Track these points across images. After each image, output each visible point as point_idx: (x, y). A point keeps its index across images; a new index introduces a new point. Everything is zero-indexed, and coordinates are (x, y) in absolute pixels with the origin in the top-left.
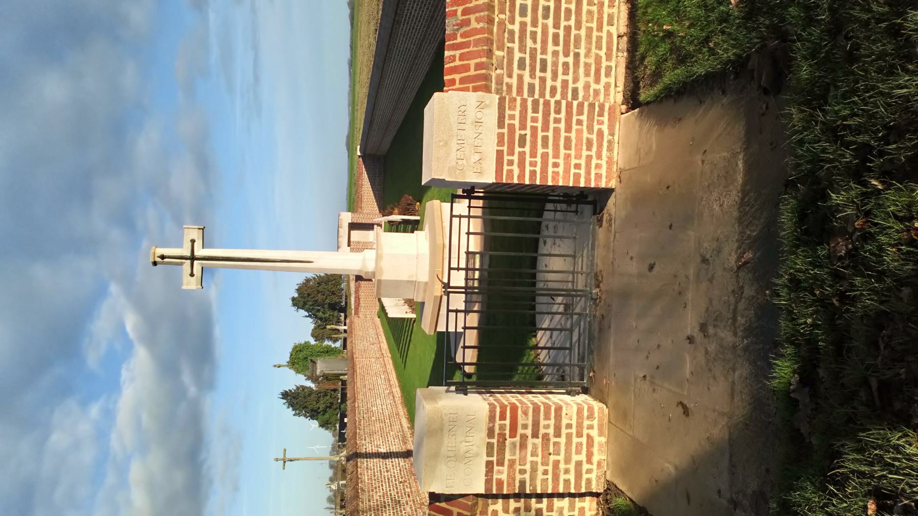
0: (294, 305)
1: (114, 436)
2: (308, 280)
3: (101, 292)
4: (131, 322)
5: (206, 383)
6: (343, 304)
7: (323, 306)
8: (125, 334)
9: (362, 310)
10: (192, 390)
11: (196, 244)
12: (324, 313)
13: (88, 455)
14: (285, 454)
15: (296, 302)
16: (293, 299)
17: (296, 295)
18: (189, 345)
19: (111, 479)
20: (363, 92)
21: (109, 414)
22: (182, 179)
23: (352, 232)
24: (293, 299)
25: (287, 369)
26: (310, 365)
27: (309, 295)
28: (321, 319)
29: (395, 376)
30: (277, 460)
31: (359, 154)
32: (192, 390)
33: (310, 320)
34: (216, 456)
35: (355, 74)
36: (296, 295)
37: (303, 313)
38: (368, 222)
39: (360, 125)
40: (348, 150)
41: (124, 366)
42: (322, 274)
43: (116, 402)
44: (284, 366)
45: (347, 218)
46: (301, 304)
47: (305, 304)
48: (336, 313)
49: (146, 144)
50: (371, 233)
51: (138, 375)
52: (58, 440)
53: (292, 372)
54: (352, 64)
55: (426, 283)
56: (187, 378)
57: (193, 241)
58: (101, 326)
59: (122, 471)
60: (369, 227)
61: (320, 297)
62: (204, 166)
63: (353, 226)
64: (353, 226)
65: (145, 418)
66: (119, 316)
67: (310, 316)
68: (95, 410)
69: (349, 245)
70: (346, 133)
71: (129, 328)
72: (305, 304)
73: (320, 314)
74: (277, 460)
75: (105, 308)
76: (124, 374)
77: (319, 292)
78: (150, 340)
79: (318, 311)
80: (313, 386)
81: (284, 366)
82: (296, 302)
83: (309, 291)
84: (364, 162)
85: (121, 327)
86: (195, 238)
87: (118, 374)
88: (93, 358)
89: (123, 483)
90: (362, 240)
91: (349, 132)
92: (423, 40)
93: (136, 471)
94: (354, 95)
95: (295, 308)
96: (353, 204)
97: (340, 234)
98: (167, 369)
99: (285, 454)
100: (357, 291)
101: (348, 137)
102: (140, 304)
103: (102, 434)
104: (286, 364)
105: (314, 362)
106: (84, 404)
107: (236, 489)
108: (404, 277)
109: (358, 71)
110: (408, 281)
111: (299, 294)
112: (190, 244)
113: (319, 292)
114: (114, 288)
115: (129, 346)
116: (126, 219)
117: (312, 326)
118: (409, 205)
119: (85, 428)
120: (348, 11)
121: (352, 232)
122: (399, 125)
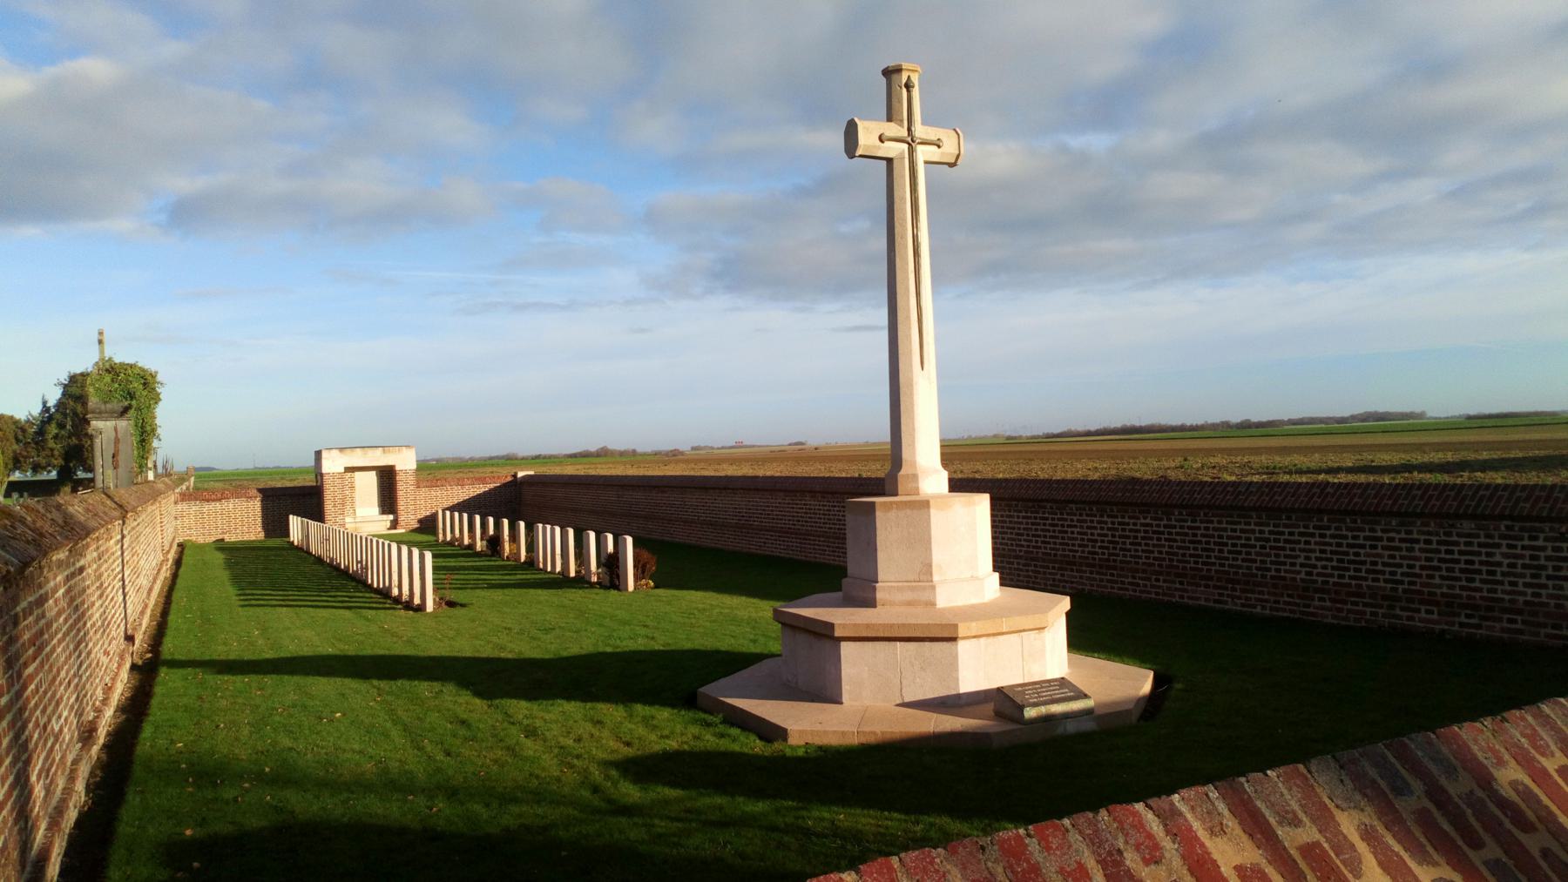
4: (96, 69)
8: (74, 53)
12: (56, 437)
22: (364, 180)
23: (373, 473)
26: (117, 405)
28: (41, 432)
31: (520, 474)
33: (36, 410)
37: (54, 396)
39: (569, 470)
44: (102, 351)
45: (405, 462)
48: (60, 462)
49: (450, 124)
50: (376, 510)
54: (585, 455)
55: (933, 604)
62: (388, 218)
64: (387, 477)
67: (46, 409)
73: (53, 429)
79: (61, 426)
81: (102, 351)
90: (358, 495)
94: (478, 466)
95: (64, 379)
96: (431, 472)
97: (370, 452)
108: (938, 556)
110: (930, 566)
114: (173, 50)
120: (593, 448)
121: (373, 473)
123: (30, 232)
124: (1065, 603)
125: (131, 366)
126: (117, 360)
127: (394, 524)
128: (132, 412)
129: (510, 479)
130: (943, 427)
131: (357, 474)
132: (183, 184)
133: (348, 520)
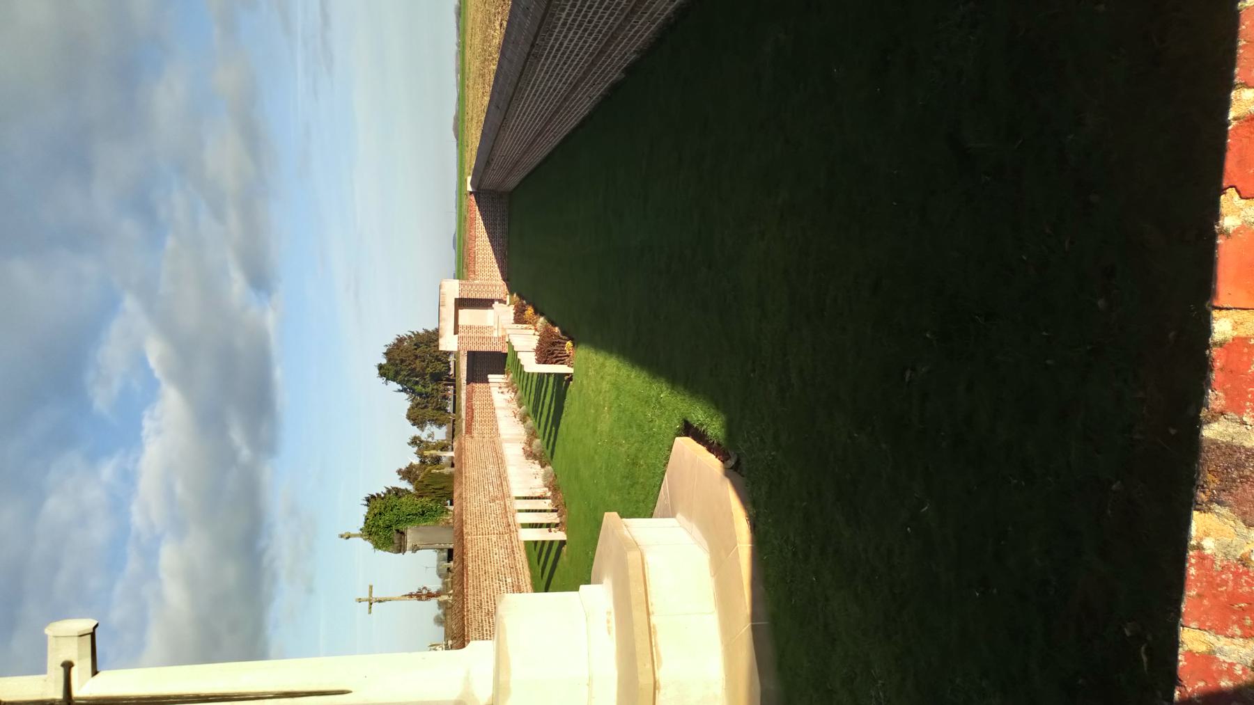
0: (382, 375)
1: (135, 508)
2: (401, 340)
3: (110, 305)
4: (155, 351)
5: (265, 445)
6: (452, 372)
7: (423, 376)
9: (477, 426)
10: (245, 453)
11: (74, 672)
12: (424, 387)
13: (99, 532)
14: (371, 592)
15: (370, 500)
16: (381, 367)
17: (384, 361)
18: (241, 394)
19: (133, 565)
20: (480, 100)
21: (128, 477)
22: (222, 155)
24: (381, 367)
25: (361, 540)
26: (396, 537)
27: (402, 361)
28: (420, 395)
29: (528, 580)
30: (360, 600)
31: (470, 188)
32: (245, 453)
33: (404, 396)
34: (282, 543)
35: (464, 31)
36: (384, 361)
37: (395, 386)
38: (485, 296)
40: (457, 137)
41: (147, 413)
42: (421, 331)
43: (137, 460)
44: (355, 536)
45: (453, 289)
46: (391, 374)
47: (397, 373)
49: (168, 97)
50: (489, 311)
51: (166, 433)
52: (56, 507)
53: (368, 545)
56: (237, 435)
57: (68, 666)
58: (112, 353)
59: (149, 555)
60: (486, 304)
61: (418, 364)
62: (253, 138)
63: (461, 303)
64: (461, 303)
65: (179, 489)
66: (135, 344)
67: (404, 390)
68: (107, 470)
69: (456, 332)
70: (454, 113)
71: (153, 361)
72: (397, 373)
73: (419, 388)
74: (360, 600)
75: (115, 329)
76: (147, 424)
77: (416, 357)
78: (183, 378)
79: (417, 383)
80: (410, 488)
81: (355, 536)
82: (383, 371)
83: (403, 356)
84: (478, 202)
85: (142, 361)
86: (70, 655)
87: (139, 427)
88: (102, 400)
89: (150, 573)
90: (477, 324)
91: (458, 112)
92: (582, 79)
93: (168, 556)
96: (463, 268)
97: (443, 316)
98: (209, 421)
99: (371, 592)
100: (469, 399)
101: (457, 119)
102: (167, 327)
103: (118, 505)
104: (359, 532)
105: (402, 534)
106: (93, 458)
107: (310, 591)
109: (469, 31)
111: (389, 360)
112: (61, 671)
113: (416, 357)
114: (130, 303)
115: (152, 386)
116: (143, 206)
117: (408, 404)
118: (553, 344)
119: (93, 494)
122: (531, 167)
123: (279, 373)
124: (611, 518)
125: (367, 519)
126: (362, 525)
127: (501, 301)
128: (400, 527)
129: (473, 198)
130: (409, 647)
131: (460, 323)
132: (237, 285)
133: (495, 334)
